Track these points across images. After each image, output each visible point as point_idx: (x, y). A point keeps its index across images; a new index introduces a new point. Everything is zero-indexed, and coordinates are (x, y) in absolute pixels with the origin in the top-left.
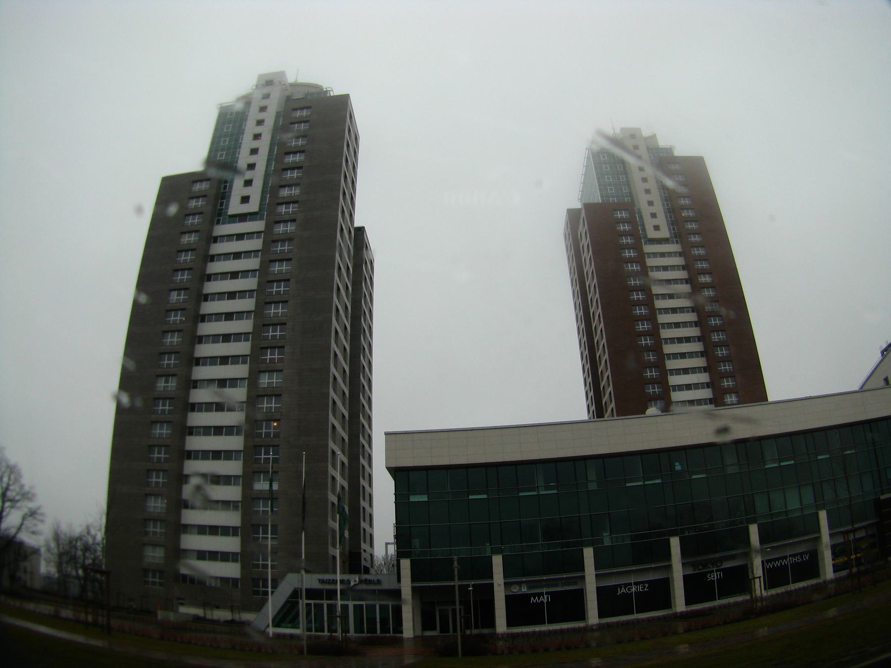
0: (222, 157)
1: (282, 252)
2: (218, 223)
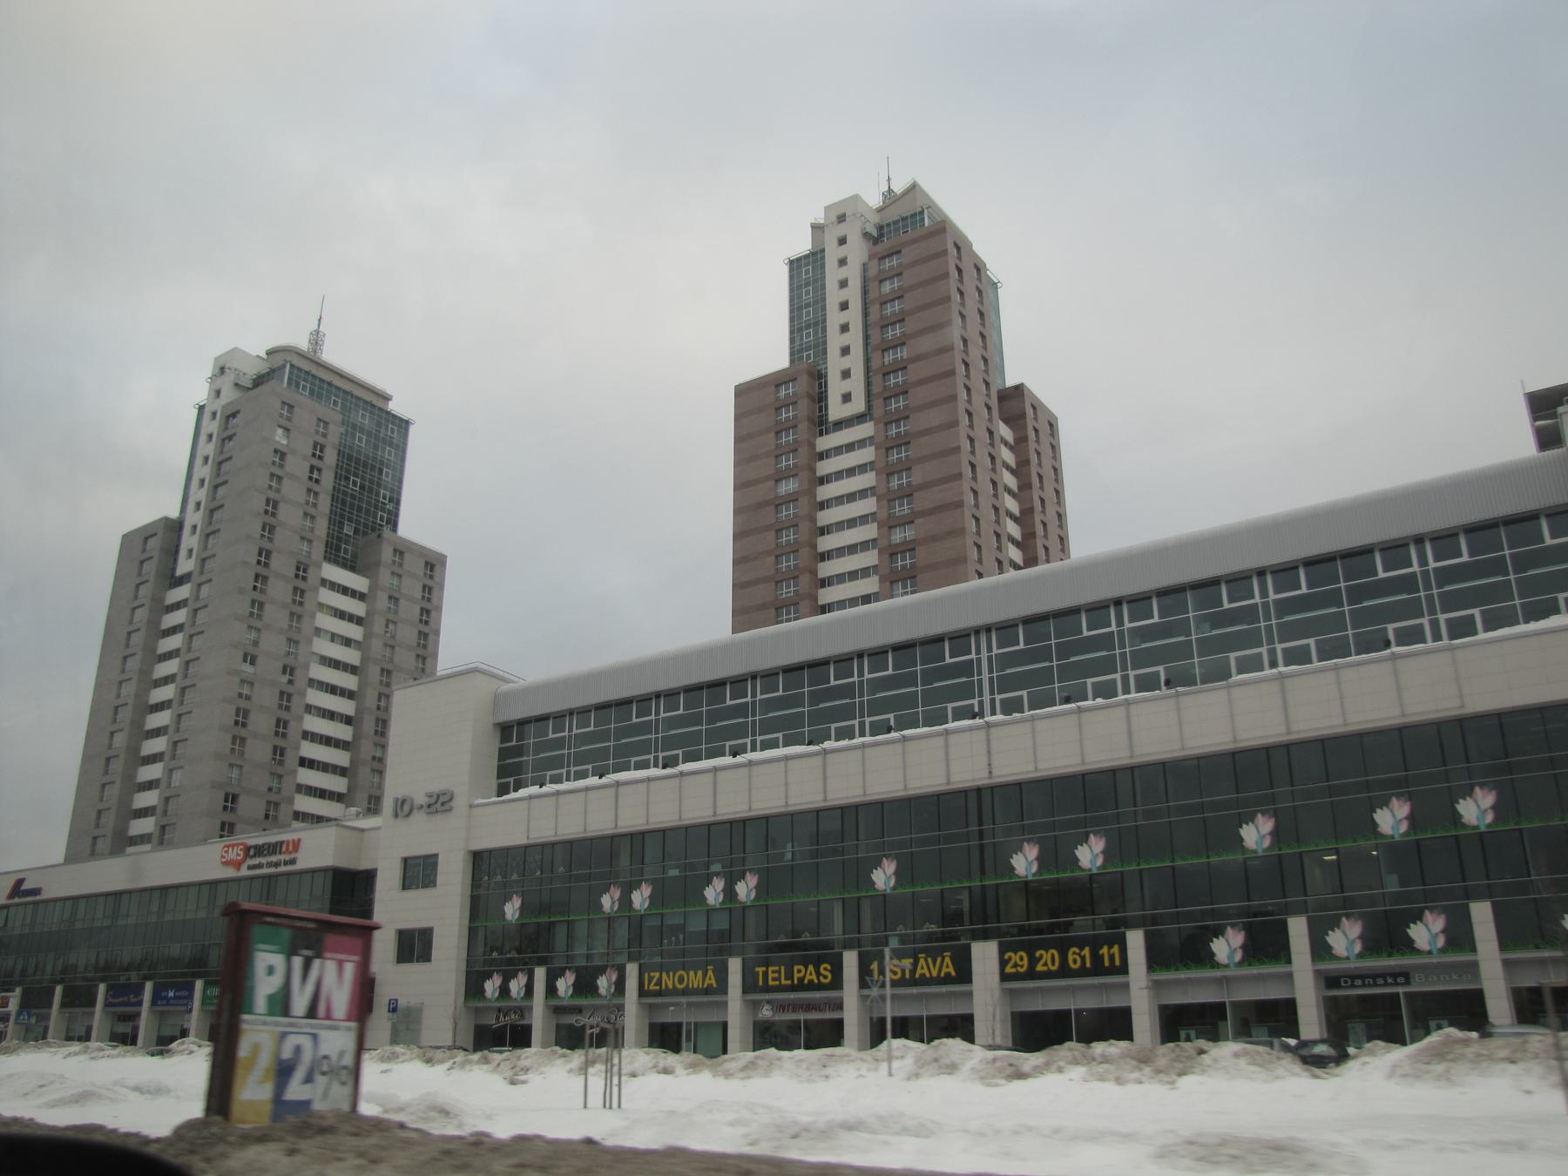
0: (808, 315)
1: (895, 360)
2: (821, 434)
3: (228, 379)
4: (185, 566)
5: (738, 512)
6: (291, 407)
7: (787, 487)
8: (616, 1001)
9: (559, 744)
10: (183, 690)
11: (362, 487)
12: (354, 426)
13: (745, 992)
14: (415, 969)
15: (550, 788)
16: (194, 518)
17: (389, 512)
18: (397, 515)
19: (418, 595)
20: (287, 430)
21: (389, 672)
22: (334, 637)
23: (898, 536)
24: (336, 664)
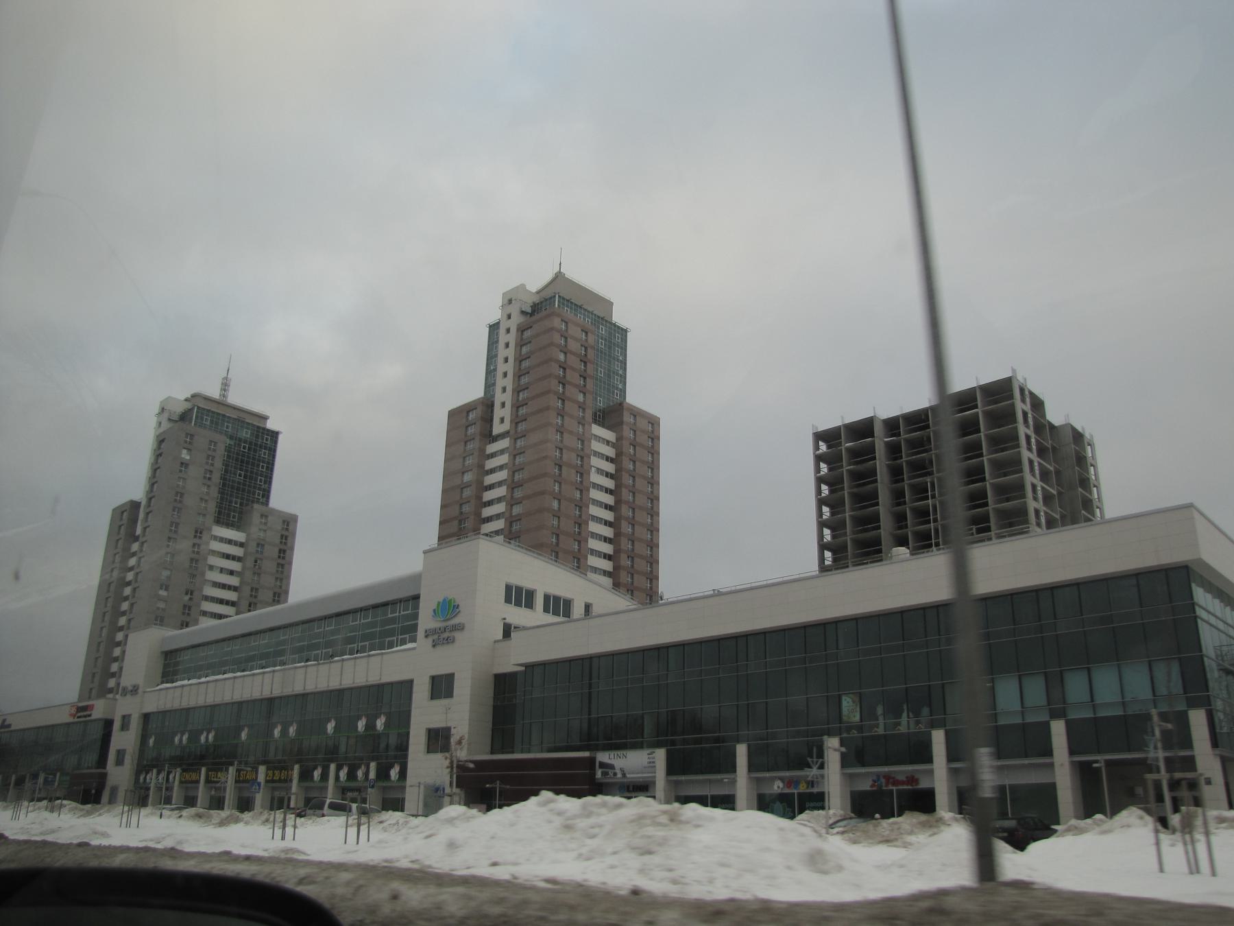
3: (166, 415)
4: (139, 531)
5: (444, 491)
6: (192, 436)
7: (468, 477)
8: (322, 784)
9: (393, 621)
10: (132, 605)
11: (245, 477)
12: (240, 440)
13: (750, 770)
14: (120, 768)
15: (203, 680)
16: (144, 503)
17: (264, 490)
18: (269, 492)
19: (277, 541)
20: (189, 450)
21: (257, 590)
22: (222, 570)
23: (517, 510)
24: (223, 586)
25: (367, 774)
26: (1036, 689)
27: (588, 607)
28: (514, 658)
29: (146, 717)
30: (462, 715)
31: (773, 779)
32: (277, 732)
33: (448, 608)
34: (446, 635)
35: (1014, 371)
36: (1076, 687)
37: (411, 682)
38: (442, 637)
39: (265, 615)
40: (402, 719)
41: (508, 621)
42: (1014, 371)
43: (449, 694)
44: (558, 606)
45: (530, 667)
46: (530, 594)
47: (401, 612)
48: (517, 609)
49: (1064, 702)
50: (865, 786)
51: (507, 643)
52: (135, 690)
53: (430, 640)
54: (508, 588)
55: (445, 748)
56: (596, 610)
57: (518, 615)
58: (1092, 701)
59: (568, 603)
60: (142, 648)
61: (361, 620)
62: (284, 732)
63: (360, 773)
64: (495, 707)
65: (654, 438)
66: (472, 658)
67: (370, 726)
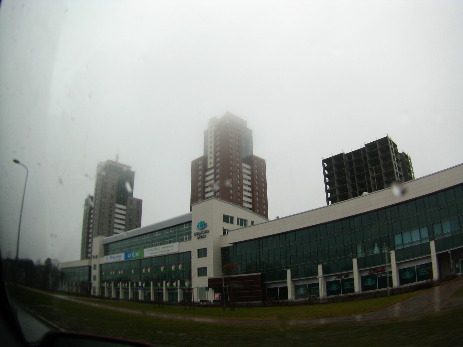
16: (94, 197)
25: (177, 284)
26: (425, 233)
27: (253, 222)
28: (228, 241)
29: (101, 265)
30: (210, 263)
31: (332, 276)
32: (144, 271)
33: (203, 225)
34: (203, 234)
35: (387, 135)
36: (437, 230)
37: (191, 252)
38: (201, 236)
39: (134, 232)
40: (188, 265)
41: (225, 228)
42: (387, 135)
43: (205, 255)
44: (242, 222)
45: (235, 244)
46: (232, 218)
47: (185, 227)
48: (228, 224)
49: (434, 235)
50: (366, 274)
51: (225, 236)
52: (97, 257)
53: (197, 236)
54: (224, 216)
55: (205, 274)
56: (255, 223)
57: (228, 226)
58: (442, 232)
59: (246, 221)
60: (97, 243)
61: (170, 231)
62: (146, 270)
63: (174, 284)
64: (222, 259)
65: (264, 167)
66: (214, 241)
67: (177, 267)
